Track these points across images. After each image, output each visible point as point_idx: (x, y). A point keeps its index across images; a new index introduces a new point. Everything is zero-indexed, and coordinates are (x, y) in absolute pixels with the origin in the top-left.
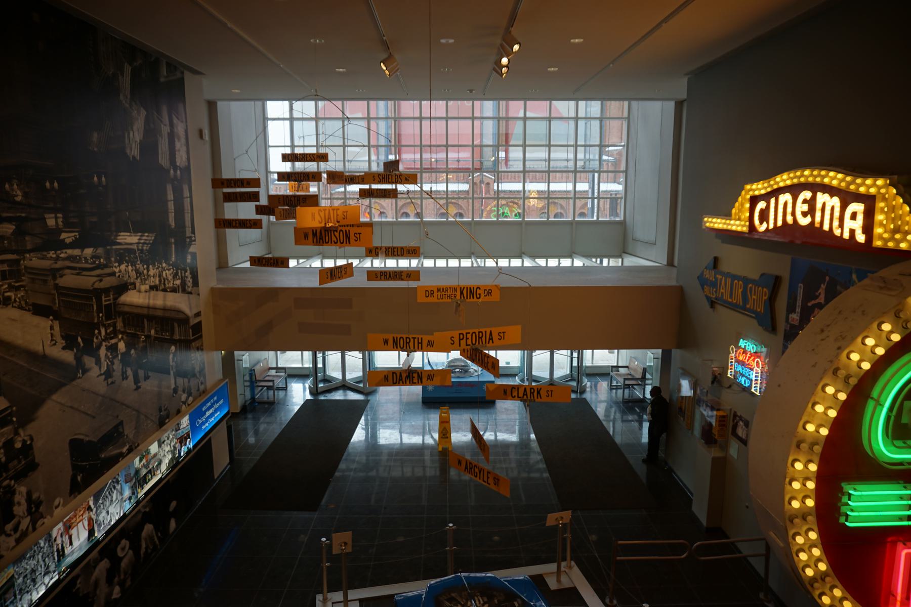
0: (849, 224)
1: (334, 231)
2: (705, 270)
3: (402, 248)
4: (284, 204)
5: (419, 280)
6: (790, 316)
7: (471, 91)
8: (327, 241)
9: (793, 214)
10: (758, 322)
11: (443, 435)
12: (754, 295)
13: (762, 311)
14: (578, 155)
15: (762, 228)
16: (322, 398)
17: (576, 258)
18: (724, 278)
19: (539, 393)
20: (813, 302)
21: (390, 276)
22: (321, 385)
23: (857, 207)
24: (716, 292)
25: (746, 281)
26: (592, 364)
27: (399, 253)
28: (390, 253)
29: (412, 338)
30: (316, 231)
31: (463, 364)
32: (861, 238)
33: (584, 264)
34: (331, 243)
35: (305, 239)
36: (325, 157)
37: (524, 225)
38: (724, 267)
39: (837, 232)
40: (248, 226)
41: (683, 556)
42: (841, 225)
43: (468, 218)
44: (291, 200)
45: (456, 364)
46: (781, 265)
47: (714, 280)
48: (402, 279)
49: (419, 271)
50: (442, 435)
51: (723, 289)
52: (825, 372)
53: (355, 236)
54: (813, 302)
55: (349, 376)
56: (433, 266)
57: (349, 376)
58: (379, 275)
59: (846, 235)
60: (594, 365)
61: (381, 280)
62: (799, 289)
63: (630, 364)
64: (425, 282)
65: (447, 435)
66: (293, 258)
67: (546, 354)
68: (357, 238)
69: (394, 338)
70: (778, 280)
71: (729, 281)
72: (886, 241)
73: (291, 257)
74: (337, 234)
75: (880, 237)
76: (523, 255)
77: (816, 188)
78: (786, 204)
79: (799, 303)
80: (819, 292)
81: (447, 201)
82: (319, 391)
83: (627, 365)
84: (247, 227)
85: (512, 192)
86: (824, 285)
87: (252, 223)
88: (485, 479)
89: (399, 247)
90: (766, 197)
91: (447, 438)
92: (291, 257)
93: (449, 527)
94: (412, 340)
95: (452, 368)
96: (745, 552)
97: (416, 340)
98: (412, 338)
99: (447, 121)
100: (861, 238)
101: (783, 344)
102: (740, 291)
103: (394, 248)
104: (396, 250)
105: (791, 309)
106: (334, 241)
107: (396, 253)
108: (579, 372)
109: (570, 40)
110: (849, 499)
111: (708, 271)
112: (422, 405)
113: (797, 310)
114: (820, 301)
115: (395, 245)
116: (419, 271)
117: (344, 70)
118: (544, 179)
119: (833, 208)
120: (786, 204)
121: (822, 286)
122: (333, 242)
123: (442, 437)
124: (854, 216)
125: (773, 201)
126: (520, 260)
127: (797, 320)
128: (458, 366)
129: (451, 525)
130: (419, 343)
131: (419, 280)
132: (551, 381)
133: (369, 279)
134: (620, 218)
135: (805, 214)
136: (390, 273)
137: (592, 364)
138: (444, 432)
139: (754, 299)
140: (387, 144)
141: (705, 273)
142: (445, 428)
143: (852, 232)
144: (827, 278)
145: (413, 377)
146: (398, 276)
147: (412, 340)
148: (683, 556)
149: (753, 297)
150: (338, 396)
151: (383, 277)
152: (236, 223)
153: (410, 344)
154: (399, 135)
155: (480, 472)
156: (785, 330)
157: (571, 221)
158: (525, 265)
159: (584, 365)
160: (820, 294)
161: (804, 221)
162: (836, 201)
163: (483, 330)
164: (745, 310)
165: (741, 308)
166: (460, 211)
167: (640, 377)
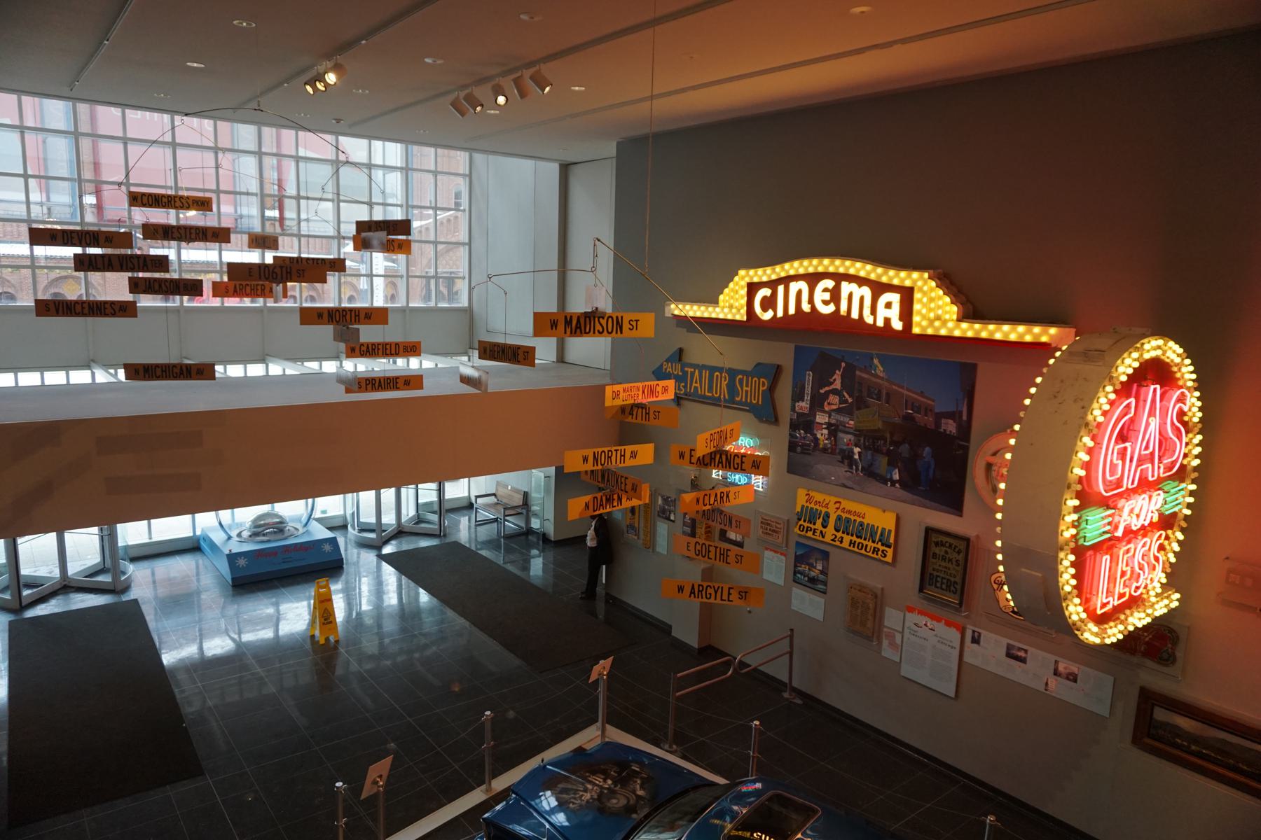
0: (882, 313)
1: (599, 318)
2: (665, 363)
3: (397, 344)
4: (260, 278)
5: (422, 388)
6: (797, 404)
7: (338, 121)
8: (587, 330)
9: (811, 301)
10: (754, 415)
11: (325, 620)
12: (747, 386)
13: (760, 403)
14: (301, 214)
15: (768, 316)
16: (30, 613)
17: (272, 362)
18: (697, 371)
19: (728, 496)
20: (827, 389)
21: (380, 385)
22: (26, 592)
23: (895, 298)
24: (685, 387)
25: (732, 373)
26: (150, 539)
27: (393, 352)
28: (380, 352)
29: (615, 450)
30: (571, 317)
31: (278, 520)
32: (897, 325)
33: (436, 365)
34: (594, 333)
35: (552, 329)
36: (207, 204)
37: (408, 311)
38: (688, 358)
39: (869, 319)
40: (107, 311)
41: (730, 672)
42: (874, 311)
43: (366, 303)
44: (273, 272)
45: (267, 521)
46: (782, 354)
47: (680, 373)
48: (398, 389)
49: (421, 377)
50: (323, 620)
51: (696, 383)
52: (1080, 427)
53: (630, 324)
54: (827, 389)
55: (73, 569)
56: (39, 383)
57: (73, 569)
58: (363, 385)
59: (880, 323)
60: (154, 540)
61: (366, 390)
62: (807, 377)
63: (497, 490)
64: (429, 389)
65: (331, 619)
66: (221, 363)
67: (372, 493)
68: (633, 326)
69: (594, 453)
70: (778, 369)
71: (706, 374)
72: (924, 328)
73: (218, 362)
74: (603, 322)
75: (919, 324)
76: (92, 364)
77: (839, 278)
78: (799, 293)
79: (808, 389)
80: (833, 378)
81: (433, 277)
82: (24, 604)
83: (494, 492)
84: (106, 315)
85: (194, 264)
86: (840, 371)
87: (117, 308)
88: (725, 597)
89: (393, 342)
90: (773, 284)
91: (331, 622)
92: (218, 362)
93: (487, 715)
94: (614, 453)
95: (260, 530)
96: (754, 665)
97: (619, 452)
98: (615, 450)
99: (401, 169)
100: (897, 325)
101: (790, 434)
102: (724, 383)
103: (387, 344)
104: (388, 347)
105: (798, 396)
106: (598, 331)
107: (388, 352)
108: (444, 508)
109: (570, 87)
110: (1087, 524)
111: (670, 364)
112: (233, 591)
113: (806, 398)
114: (835, 387)
115: (388, 340)
116: (421, 377)
117: (203, 66)
118: (240, 245)
119: (862, 299)
120: (799, 293)
121: (837, 372)
122: (596, 332)
123: (324, 624)
124: (888, 305)
125: (781, 289)
126: (88, 372)
127: (807, 408)
128: (268, 524)
129: (488, 713)
130: (621, 456)
131: (422, 388)
132: (399, 527)
133: (348, 391)
134: (464, 302)
135: (826, 303)
136: (380, 380)
137: (150, 539)
138: (325, 615)
139: (747, 391)
140: (93, 179)
141: (664, 367)
142: (326, 609)
143: (887, 321)
144: (843, 364)
145: (613, 500)
146: (391, 384)
147: (614, 453)
148: (730, 672)
149: (745, 388)
150: (41, 610)
151: (369, 387)
152: (83, 308)
153: (612, 458)
154: (45, 160)
155: (716, 592)
156: (791, 419)
157: (260, 307)
158: (424, 367)
159: (121, 543)
160: (835, 380)
161: (828, 309)
162: (866, 292)
163: (722, 429)
164: (733, 404)
165: (731, 403)
166: (311, 293)
167: (521, 503)
